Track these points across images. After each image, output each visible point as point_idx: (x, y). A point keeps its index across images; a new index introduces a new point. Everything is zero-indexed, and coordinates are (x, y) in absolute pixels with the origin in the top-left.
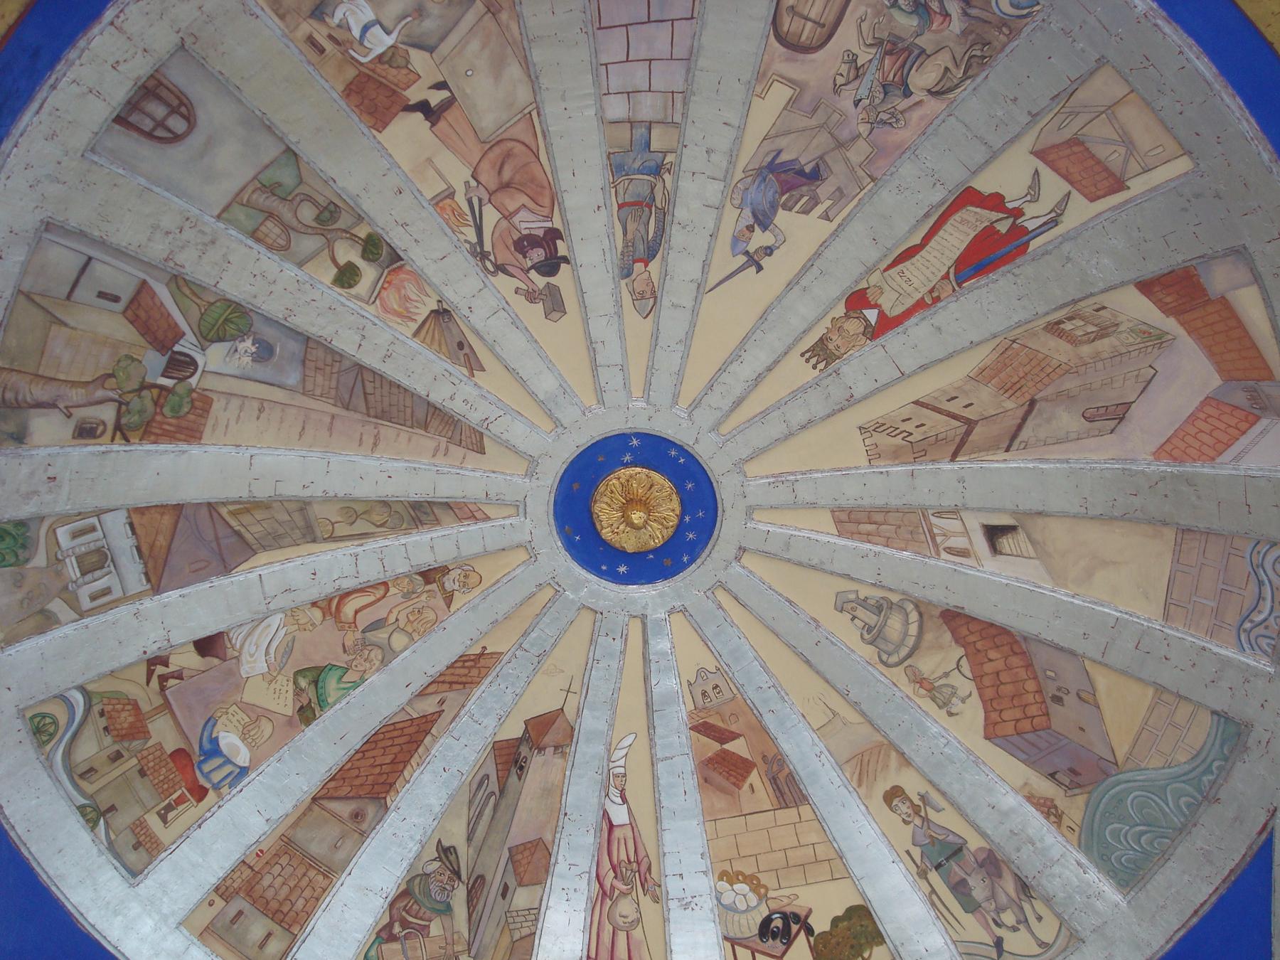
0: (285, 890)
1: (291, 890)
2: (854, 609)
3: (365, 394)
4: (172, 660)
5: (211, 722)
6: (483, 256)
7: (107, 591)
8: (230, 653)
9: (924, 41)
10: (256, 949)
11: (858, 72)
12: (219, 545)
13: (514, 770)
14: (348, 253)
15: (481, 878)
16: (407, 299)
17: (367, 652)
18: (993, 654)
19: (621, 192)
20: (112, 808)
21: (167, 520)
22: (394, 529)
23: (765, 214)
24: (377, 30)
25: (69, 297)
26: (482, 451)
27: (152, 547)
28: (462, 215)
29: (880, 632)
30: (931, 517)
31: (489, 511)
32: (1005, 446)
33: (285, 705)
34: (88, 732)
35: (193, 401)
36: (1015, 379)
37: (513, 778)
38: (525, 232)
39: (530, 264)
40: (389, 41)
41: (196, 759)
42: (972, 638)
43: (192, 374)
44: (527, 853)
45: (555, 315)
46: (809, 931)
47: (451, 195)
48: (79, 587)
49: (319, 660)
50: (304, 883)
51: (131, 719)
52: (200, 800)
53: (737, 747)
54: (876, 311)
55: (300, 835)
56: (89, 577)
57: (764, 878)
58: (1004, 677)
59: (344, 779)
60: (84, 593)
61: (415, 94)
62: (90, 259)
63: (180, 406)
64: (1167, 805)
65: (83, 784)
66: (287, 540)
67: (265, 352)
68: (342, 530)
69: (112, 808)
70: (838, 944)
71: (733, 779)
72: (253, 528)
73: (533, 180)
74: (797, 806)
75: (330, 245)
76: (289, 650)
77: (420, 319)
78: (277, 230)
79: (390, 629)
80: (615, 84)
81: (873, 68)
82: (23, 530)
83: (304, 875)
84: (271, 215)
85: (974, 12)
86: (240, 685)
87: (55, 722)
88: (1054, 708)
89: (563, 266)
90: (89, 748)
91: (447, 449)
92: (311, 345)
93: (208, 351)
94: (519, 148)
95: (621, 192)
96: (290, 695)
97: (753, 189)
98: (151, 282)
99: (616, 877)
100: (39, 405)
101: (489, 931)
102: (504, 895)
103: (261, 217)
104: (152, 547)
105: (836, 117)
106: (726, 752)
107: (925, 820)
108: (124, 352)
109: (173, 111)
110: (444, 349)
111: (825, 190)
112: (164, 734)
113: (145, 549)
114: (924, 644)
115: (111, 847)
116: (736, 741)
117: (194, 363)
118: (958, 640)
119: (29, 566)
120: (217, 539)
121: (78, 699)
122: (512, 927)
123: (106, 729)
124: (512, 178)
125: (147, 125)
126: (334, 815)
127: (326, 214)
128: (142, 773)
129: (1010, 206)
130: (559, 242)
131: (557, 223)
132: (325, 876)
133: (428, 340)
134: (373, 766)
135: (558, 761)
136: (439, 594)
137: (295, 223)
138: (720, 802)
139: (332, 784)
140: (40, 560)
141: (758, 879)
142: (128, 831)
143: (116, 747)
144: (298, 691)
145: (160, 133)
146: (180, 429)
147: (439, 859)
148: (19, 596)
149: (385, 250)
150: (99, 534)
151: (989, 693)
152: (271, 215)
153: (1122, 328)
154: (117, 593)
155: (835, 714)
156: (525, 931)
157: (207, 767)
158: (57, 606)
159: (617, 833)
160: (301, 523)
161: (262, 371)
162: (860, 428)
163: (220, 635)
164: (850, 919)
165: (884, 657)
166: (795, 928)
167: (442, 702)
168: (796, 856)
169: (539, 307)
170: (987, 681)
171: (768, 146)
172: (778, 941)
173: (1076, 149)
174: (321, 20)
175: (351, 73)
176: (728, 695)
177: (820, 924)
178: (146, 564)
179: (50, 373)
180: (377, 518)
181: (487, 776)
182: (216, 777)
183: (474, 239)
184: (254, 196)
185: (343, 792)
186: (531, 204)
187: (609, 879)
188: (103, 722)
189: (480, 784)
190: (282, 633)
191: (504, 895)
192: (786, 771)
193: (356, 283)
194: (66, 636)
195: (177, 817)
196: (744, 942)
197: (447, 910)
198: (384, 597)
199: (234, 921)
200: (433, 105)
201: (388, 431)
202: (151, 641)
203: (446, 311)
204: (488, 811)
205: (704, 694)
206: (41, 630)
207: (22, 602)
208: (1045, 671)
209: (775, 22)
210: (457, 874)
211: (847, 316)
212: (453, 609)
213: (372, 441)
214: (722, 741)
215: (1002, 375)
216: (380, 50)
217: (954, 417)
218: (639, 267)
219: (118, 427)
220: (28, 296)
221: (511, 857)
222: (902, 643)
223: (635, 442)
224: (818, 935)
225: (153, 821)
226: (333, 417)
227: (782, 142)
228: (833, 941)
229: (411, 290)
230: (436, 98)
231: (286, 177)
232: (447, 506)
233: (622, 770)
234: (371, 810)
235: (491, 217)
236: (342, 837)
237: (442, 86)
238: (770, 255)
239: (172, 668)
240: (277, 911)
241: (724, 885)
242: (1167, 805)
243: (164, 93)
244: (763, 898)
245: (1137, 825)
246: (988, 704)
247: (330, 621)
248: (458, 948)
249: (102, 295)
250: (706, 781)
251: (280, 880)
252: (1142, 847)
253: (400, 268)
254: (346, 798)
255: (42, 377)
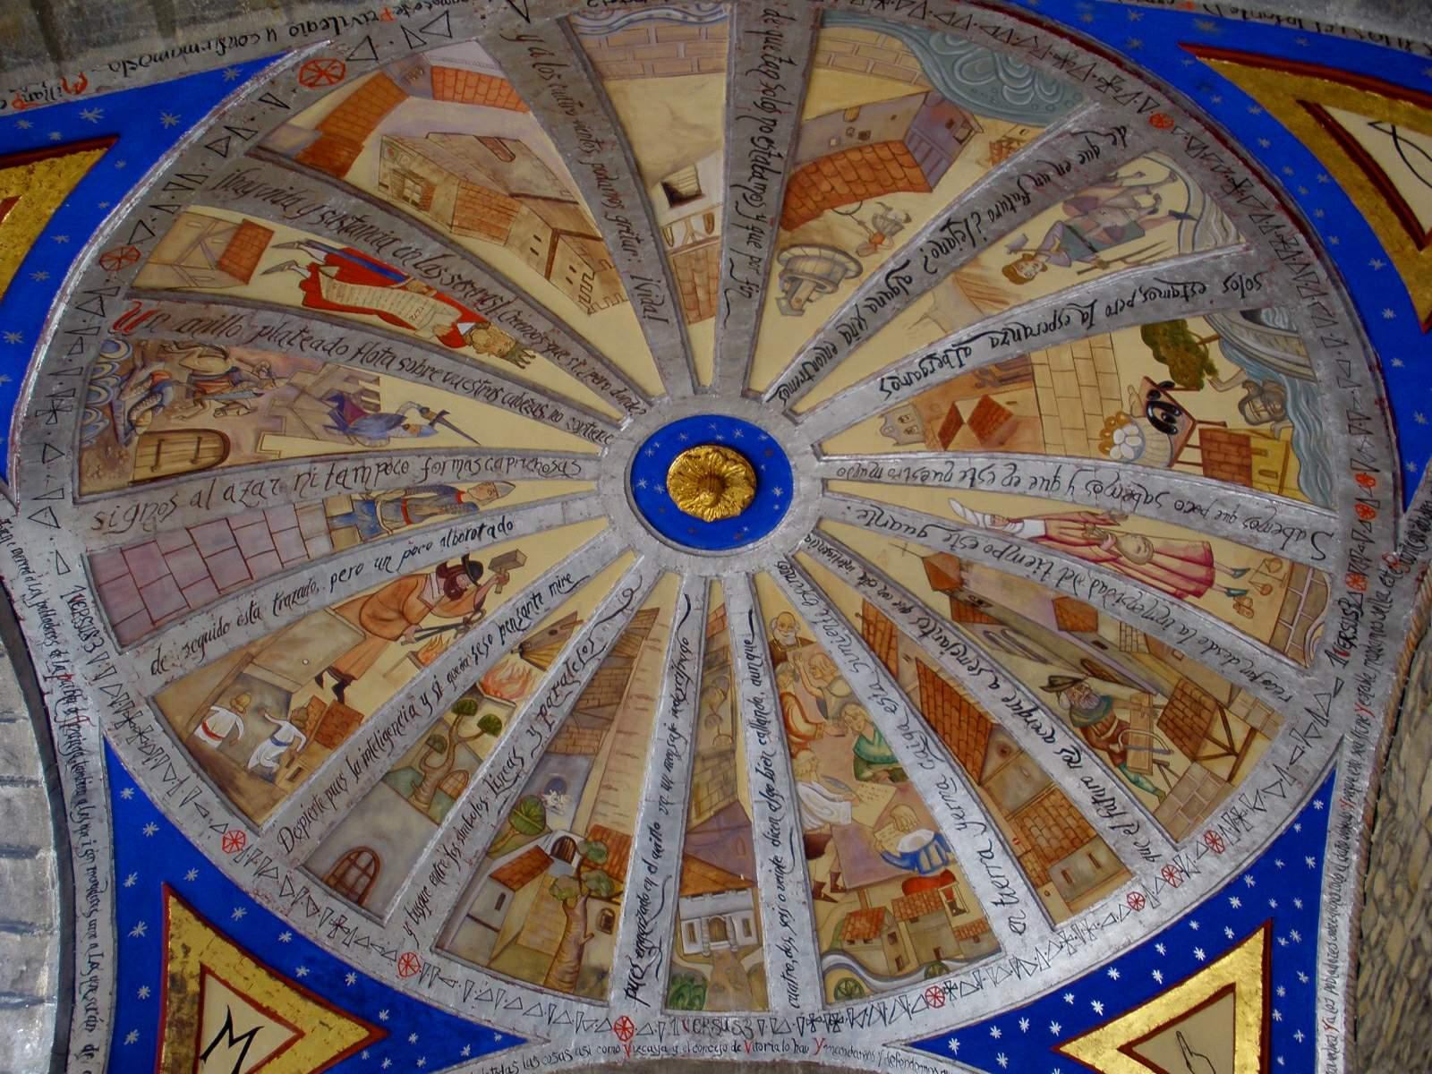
0: (1055, 829)
1: (1057, 824)
2: (799, 301)
3: (599, 706)
4: (819, 879)
5: (886, 856)
6: (467, 622)
7: (746, 923)
8: (825, 831)
9: (183, 377)
10: (1099, 871)
11: (230, 405)
12: (726, 829)
13: (982, 609)
14: (471, 726)
15: (1083, 662)
16: (510, 677)
17: (847, 718)
18: (825, 187)
19: (395, 525)
20: (937, 952)
21: (695, 867)
22: (730, 684)
23: (388, 422)
24: (278, 736)
25: (496, 930)
26: (656, 611)
27: (715, 882)
28: (431, 644)
29: (820, 278)
30: (676, 246)
31: (716, 603)
32: (572, 206)
33: (886, 792)
34: (864, 956)
35: (595, 841)
36: (494, 212)
37: (991, 611)
38: (443, 593)
39: (472, 585)
40: (286, 725)
41: (915, 873)
42: (811, 204)
43: (571, 840)
44: (1065, 616)
45: (520, 559)
46: (1168, 386)
47: (415, 654)
48: (736, 943)
49: (849, 759)
50: (1054, 813)
51: (864, 920)
52: (954, 879)
53: (966, 409)
54: (459, 325)
55: (1009, 803)
56: (730, 935)
57: (1110, 411)
58: (852, 176)
59: (967, 755)
60: (742, 940)
61: (329, 697)
62: (468, 915)
63: (599, 850)
64: (962, 55)
65: (908, 969)
66: (730, 774)
67: (558, 785)
68: (726, 728)
69: (937, 952)
70: (1183, 362)
71: (1002, 419)
72: (713, 800)
73: (394, 595)
74: (1032, 364)
75: (463, 741)
76: (835, 782)
77: (529, 666)
78: (451, 781)
79: (828, 695)
80: (297, 552)
81: (223, 396)
82: (679, 979)
83: (1046, 810)
84: (438, 787)
85: (139, 363)
86: (858, 828)
87: (846, 980)
88: (874, 137)
89: (471, 558)
90: (878, 957)
91: (653, 640)
92: (552, 749)
93: (553, 827)
94: (367, 610)
95: (395, 525)
96: (876, 786)
97: (368, 434)
98: (490, 871)
99: (1099, 545)
100: (580, 957)
101: (1131, 670)
102: (1103, 647)
103: (440, 793)
104: (715, 882)
105: (277, 403)
106: (971, 422)
107: (1039, 252)
108: (546, 891)
109: (354, 863)
110: (556, 646)
111: (350, 388)
112: (886, 896)
113: (717, 888)
114: (828, 241)
115: (970, 960)
116: (960, 409)
117: (562, 840)
118: (815, 215)
119: (709, 978)
120: (720, 830)
121: (831, 959)
122: (1134, 649)
123: (866, 941)
124: (394, 610)
125: (365, 880)
126: (998, 770)
127: (437, 746)
128: (914, 920)
129: (308, 274)
130: (449, 566)
131: (434, 569)
132: (1052, 793)
133: (549, 659)
134: (960, 727)
135: (975, 570)
136: (799, 650)
137: (446, 768)
138: (1025, 436)
139: (969, 766)
140: (706, 970)
141: (1110, 419)
142: (961, 943)
143: (885, 936)
144: (875, 779)
145: (371, 871)
146: (618, 852)
147: (1058, 693)
148: (731, 990)
149: (468, 698)
150: (696, 922)
151: (873, 188)
152: (438, 787)
153: (396, 166)
154: (750, 915)
155: (926, 316)
156: (1141, 640)
157: (925, 865)
158: (747, 963)
159: (1053, 533)
160: (716, 761)
161: (574, 787)
162: (589, 313)
163: (804, 838)
164: (1156, 343)
165: (851, 274)
166: (1163, 398)
167: (907, 658)
168: (1086, 376)
169: (513, 573)
170: (861, 190)
171: (324, 434)
172: (1177, 418)
173: (226, 262)
174: (275, 775)
175: (316, 746)
176: (910, 410)
177: (1162, 374)
178: (729, 889)
179: (556, 946)
180: (718, 698)
181: (986, 633)
182: (937, 860)
183: (453, 631)
184: (422, 799)
185: (979, 759)
186: (416, 593)
187: (1099, 551)
188: (859, 943)
189: (993, 640)
190: (816, 786)
191: (1103, 647)
192: (993, 369)
193: (496, 718)
194: (772, 962)
195: (962, 900)
196: (1177, 449)
197: (1108, 701)
198: (795, 697)
199: (1069, 880)
200: (336, 682)
201: (634, 687)
202: (796, 893)
203: (521, 646)
204: (1020, 640)
205: (909, 432)
206: (763, 980)
207: (736, 989)
208: (830, 147)
209: (209, 467)
210: (1075, 681)
211: (472, 343)
212: (814, 639)
213: (644, 701)
214: (960, 423)
215: (493, 222)
216: (294, 729)
217: (553, 247)
218: (464, 499)
219: (609, 899)
220: (493, 960)
221: (1068, 630)
222: (832, 260)
223: (642, 483)
224: (1172, 376)
225: (959, 921)
226: (619, 731)
227: (316, 428)
228: (1181, 366)
229: (502, 675)
230: (330, 681)
231: (405, 779)
232: (709, 640)
233: (988, 518)
234: (1001, 739)
235: (431, 621)
236: (1021, 769)
237: (319, 680)
238: (428, 409)
239: (828, 880)
240: (1072, 842)
241: (1114, 452)
242: (962, 55)
243: (340, 871)
244: (1130, 419)
245: (999, 78)
246: (885, 190)
247: (811, 745)
248: (1145, 702)
249: (498, 907)
250: (1002, 443)
251: (1045, 831)
252: (1027, 77)
253: (482, 685)
254: (985, 757)
255: (557, 953)
